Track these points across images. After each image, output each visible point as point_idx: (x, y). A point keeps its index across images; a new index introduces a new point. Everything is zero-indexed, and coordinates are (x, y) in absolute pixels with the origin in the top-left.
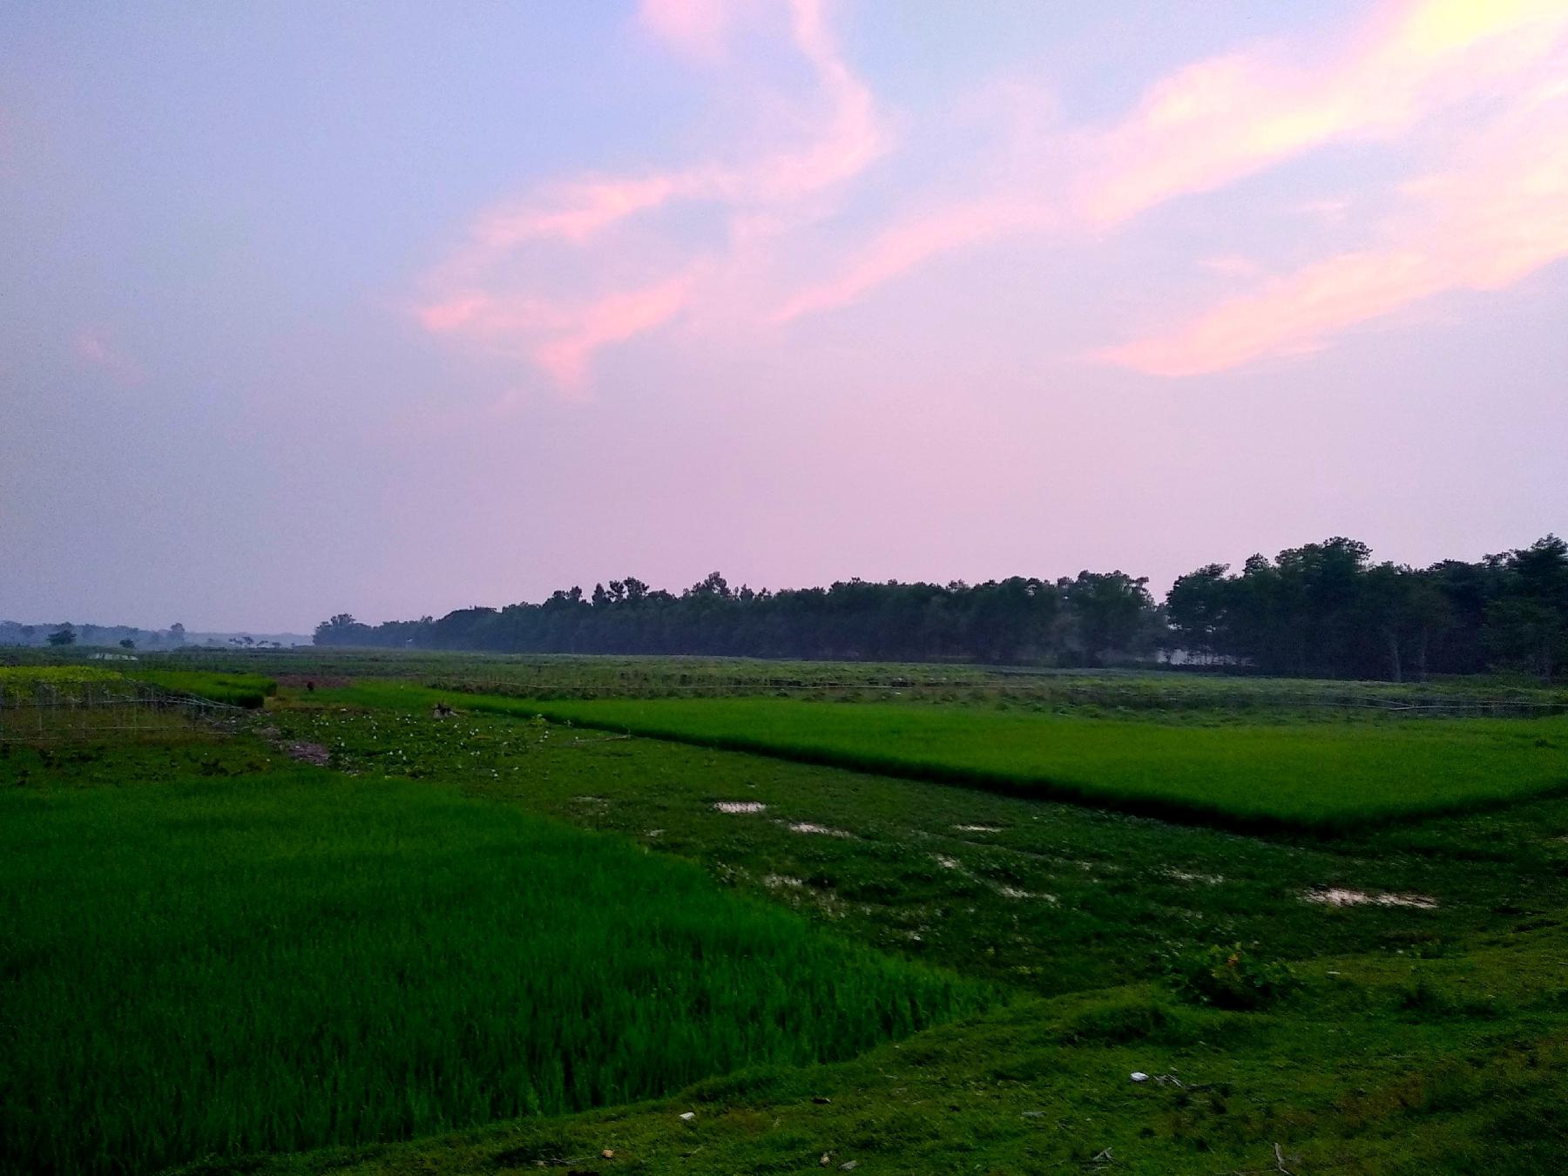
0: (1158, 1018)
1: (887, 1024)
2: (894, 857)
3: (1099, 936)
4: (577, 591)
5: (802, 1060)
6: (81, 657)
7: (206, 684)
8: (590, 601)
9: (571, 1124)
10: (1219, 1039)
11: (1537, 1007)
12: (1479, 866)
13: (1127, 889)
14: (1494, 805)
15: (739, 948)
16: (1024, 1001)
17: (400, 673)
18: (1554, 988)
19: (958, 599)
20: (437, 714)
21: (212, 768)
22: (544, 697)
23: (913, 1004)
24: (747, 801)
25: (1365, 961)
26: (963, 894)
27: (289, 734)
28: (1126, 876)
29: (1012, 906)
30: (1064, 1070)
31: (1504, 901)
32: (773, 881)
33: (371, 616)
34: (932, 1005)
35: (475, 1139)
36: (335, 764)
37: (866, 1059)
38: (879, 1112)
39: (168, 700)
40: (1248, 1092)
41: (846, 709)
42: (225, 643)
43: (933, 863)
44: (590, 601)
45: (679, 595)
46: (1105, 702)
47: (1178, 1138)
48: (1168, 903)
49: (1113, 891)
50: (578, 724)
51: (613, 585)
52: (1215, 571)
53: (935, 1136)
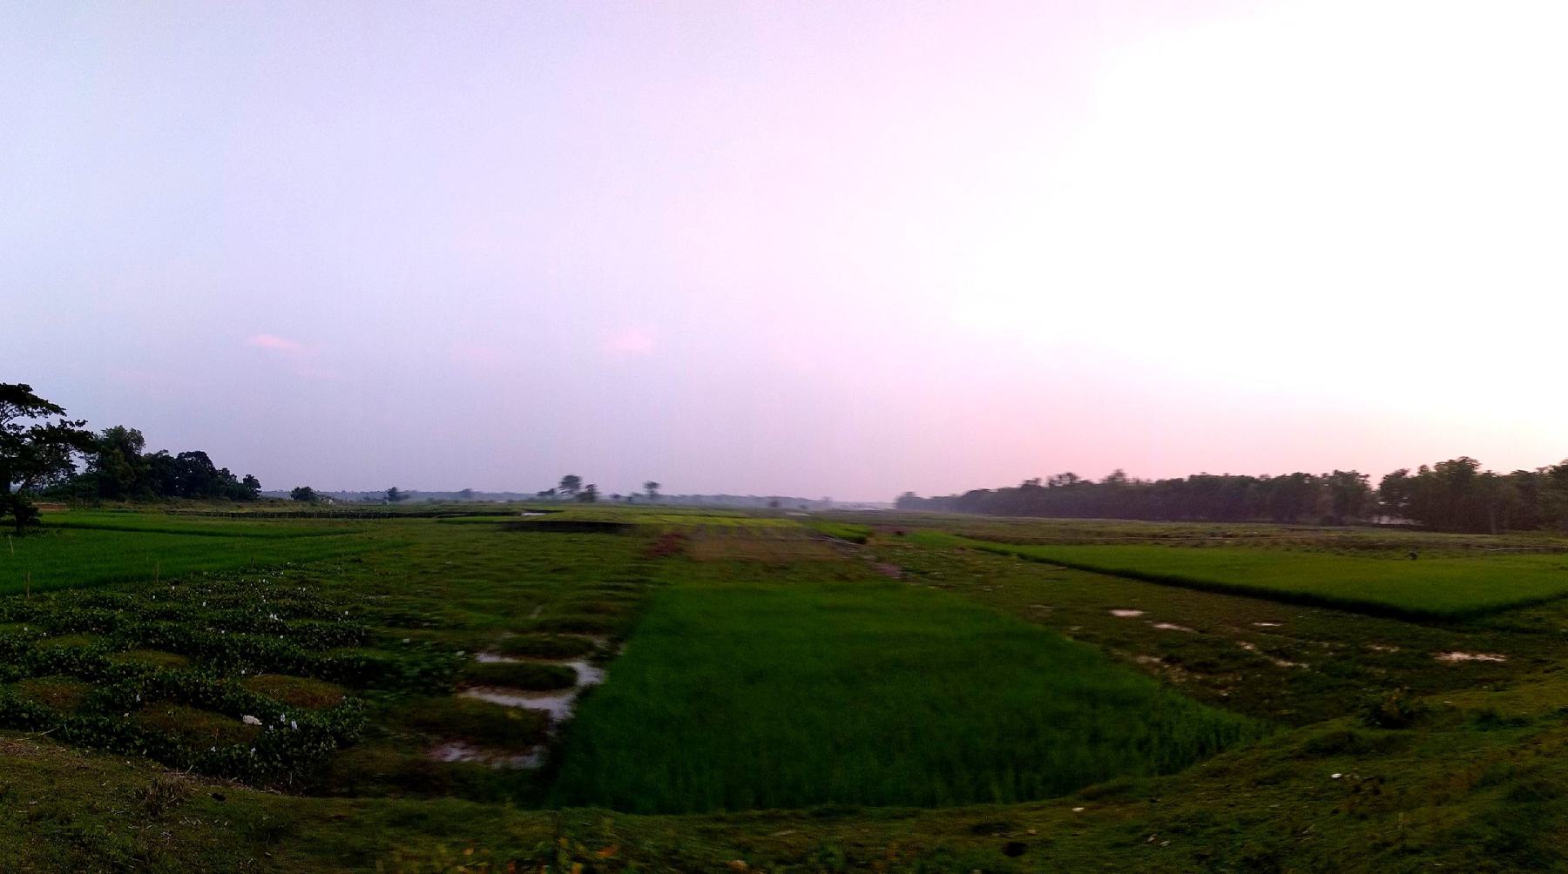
0: (1351, 737)
1: (1202, 750)
2: (1217, 644)
3: (1330, 687)
5: (1150, 773)
7: (838, 530)
9: (1018, 810)
10: (1384, 748)
11: (1547, 718)
12: (1526, 636)
13: (1346, 658)
14: (1537, 603)
15: (1122, 702)
16: (1282, 732)
18: (1557, 706)
19: (1265, 485)
21: (842, 577)
22: (1019, 542)
23: (1218, 736)
24: (1131, 609)
25: (1465, 695)
26: (1255, 665)
27: (880, 560)
28: (1347, 650)
29: (1282, 672)
30: (1295, 775)
31: (1540, 656)
32: (1143, 659)
33: (925, 493)
34: (1229, 737)
35: (964, 814)
36: (904, 579)
37: (1187, 773)
38: (1188, 808)
40: (1394, 779)
41: (1195, 552)
43: (1239, 647)
46: (1344, 546)
47: (1352, 812)
48: (1368, 665)
49: (1340, 659)
52: (1404, 472)
53: (1216, 825)
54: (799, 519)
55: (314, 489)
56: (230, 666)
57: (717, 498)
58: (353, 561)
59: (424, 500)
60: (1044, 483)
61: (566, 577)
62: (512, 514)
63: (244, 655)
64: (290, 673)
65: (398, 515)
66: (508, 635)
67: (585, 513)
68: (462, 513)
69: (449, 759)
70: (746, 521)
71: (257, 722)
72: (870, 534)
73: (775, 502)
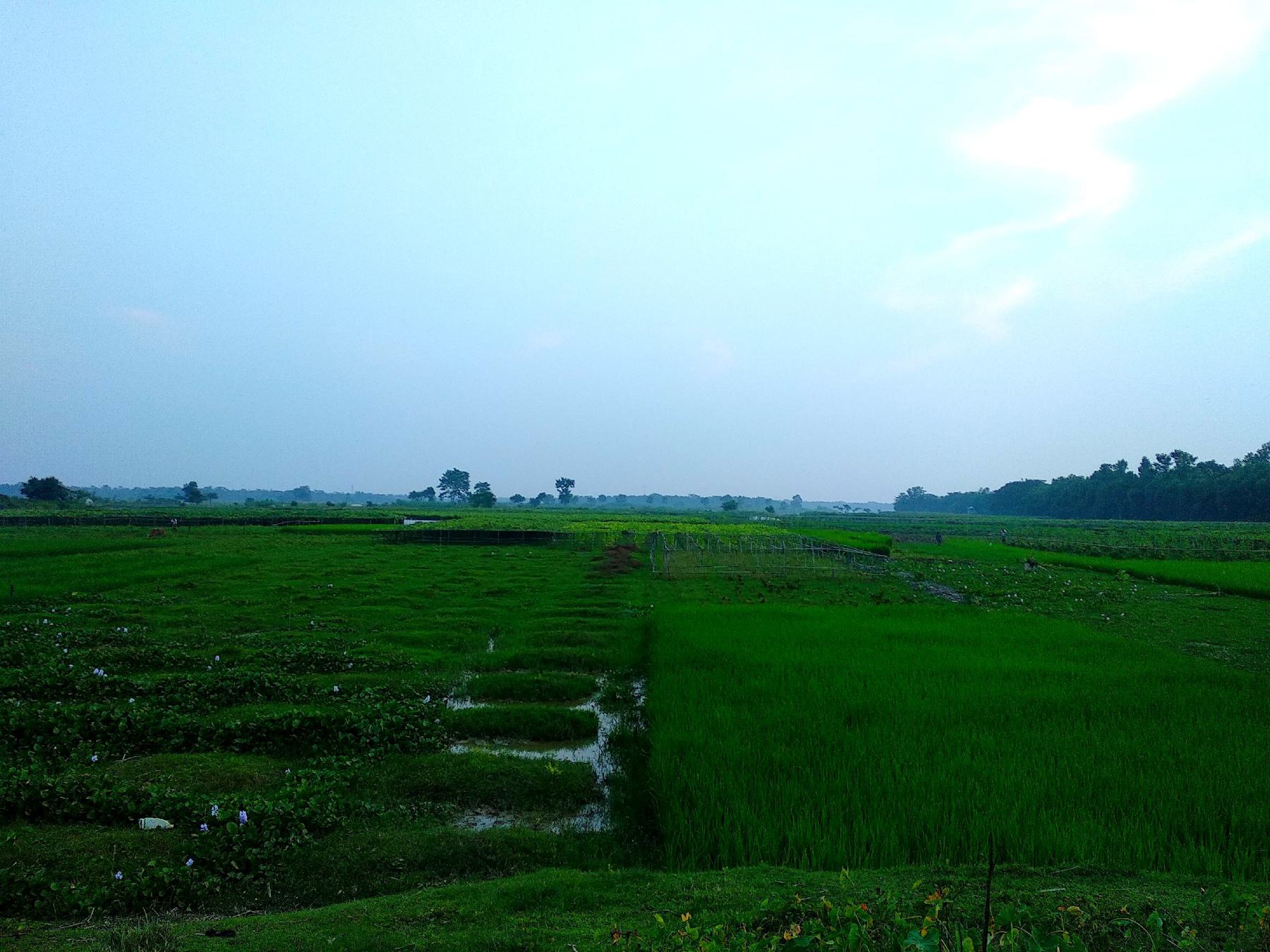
4: (1123, 464)
6: (744, 518)
8: (1136, 472)
17: (977, 533)
20: (1027, 566)
33: (938, 488)
39: (830, 550)
42: (831, 509)
44: (1136, 472)
45: (1229, 464)
50: (1161, 580)
51: (1159, 458)
54: (784, 523)
55: (67, 482)
56: (66, 753)
57: (650, 498)
58: (182, 586)
59: (321, 502)
60: (1133, 467)
61: (507, 601)
62: (391, 521)
63: (89, 734)
64: (177, 749)
65: (217, 522)
66: (467, 677)
67: (475, 519)
68: (313, 521)
69: (479, 828)
70: (714, 529)
71: (166, 824)
72: (890, 542)
73: (730, 504)
